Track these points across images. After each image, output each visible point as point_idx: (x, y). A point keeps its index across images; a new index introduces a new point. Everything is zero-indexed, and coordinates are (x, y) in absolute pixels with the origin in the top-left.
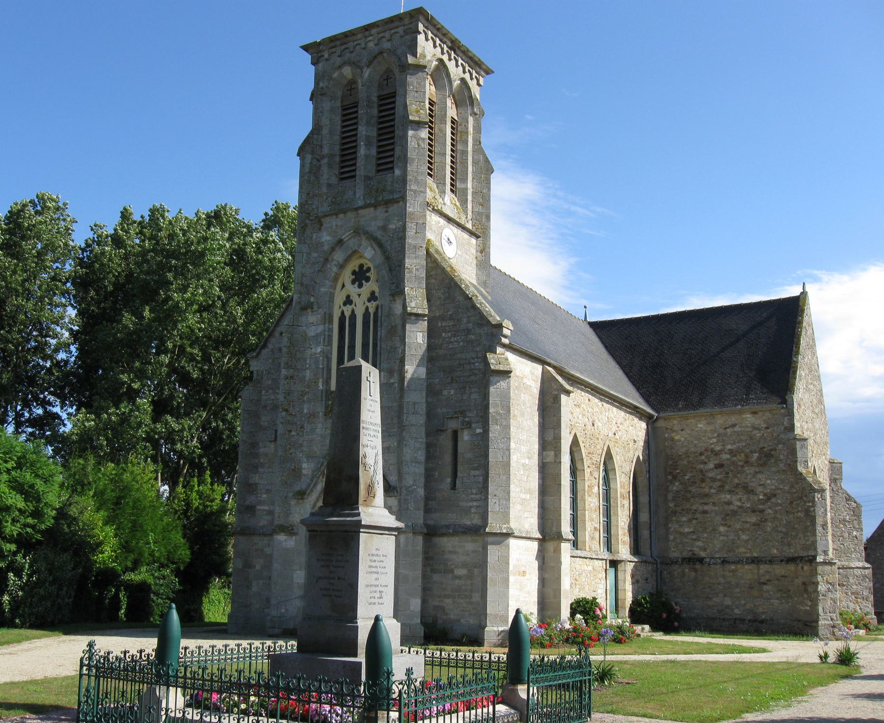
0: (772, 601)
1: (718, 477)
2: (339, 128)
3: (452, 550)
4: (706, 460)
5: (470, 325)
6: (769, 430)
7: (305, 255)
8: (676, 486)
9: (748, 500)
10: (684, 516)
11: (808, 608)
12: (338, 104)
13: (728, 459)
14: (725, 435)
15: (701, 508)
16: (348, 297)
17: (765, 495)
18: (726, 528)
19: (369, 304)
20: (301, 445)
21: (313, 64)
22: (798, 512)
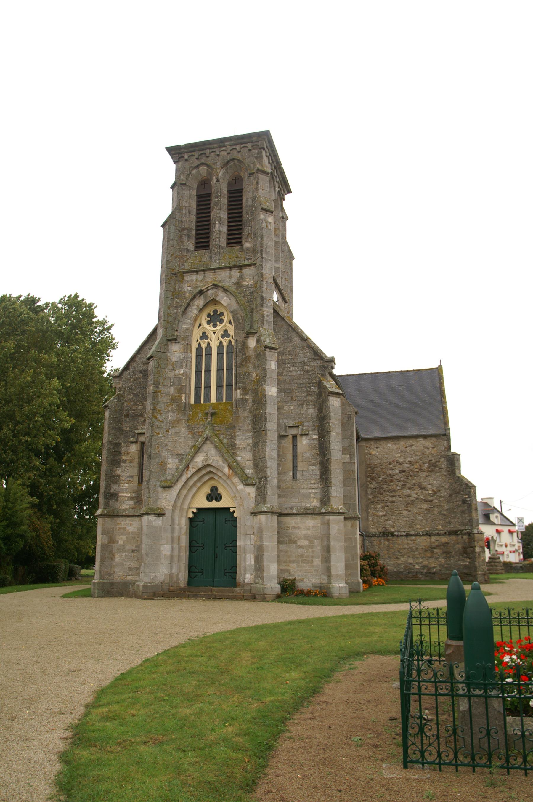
0: (440, 559)
1: (402, 479)
2: (195, 210)
3: (295, 526)
4: (393, 468)
5: (306, 359)
6: (435, 449)
7: (169, 299)
8: (373, 485)
9: (422, 493)
10: (379, 504)
11: (468, 563)
12: (194, 193)
13: (408, 467)
14: (406, 451)
15: (390, 499)
16: (204, 333)
17: (433, 490)
18: (407, 512)
19: (223, 340)
20: (167, 445)
21: (175, 162)
22: (457, 501)
